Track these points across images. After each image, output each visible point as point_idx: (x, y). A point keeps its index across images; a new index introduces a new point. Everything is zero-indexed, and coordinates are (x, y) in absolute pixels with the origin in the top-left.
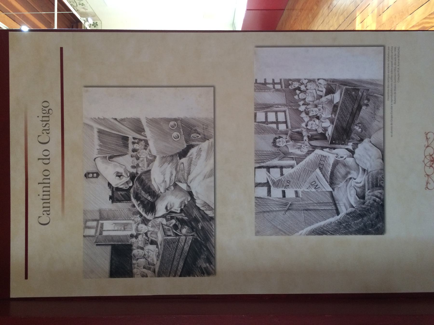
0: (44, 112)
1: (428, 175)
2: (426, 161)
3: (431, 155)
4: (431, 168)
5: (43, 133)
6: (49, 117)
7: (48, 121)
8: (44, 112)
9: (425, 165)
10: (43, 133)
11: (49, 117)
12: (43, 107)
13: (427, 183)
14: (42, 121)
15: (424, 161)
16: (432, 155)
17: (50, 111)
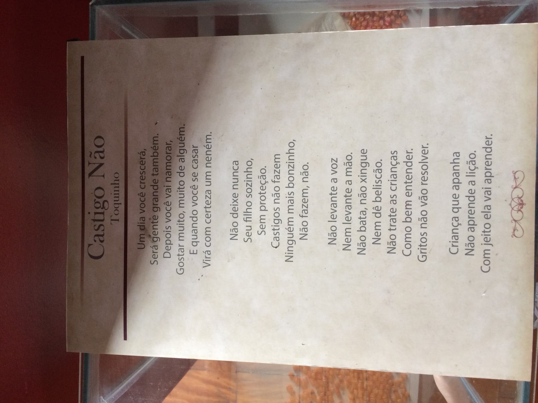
0: (98, 205)
1: (515, 221)
2: (514, 204)
3: (520, 198)
4: (519, 212)
5: (95, 241)
6: (103, 213)
7: (103, 220)
8: (98, 205)
9: (513, 209)
10: (95, 241)
11: (103, 213)
12: (96, 198)
13: (514, 230)
14: (94, 220)
15: (510, 205)
16: (522, 197)
17: (106, 203)
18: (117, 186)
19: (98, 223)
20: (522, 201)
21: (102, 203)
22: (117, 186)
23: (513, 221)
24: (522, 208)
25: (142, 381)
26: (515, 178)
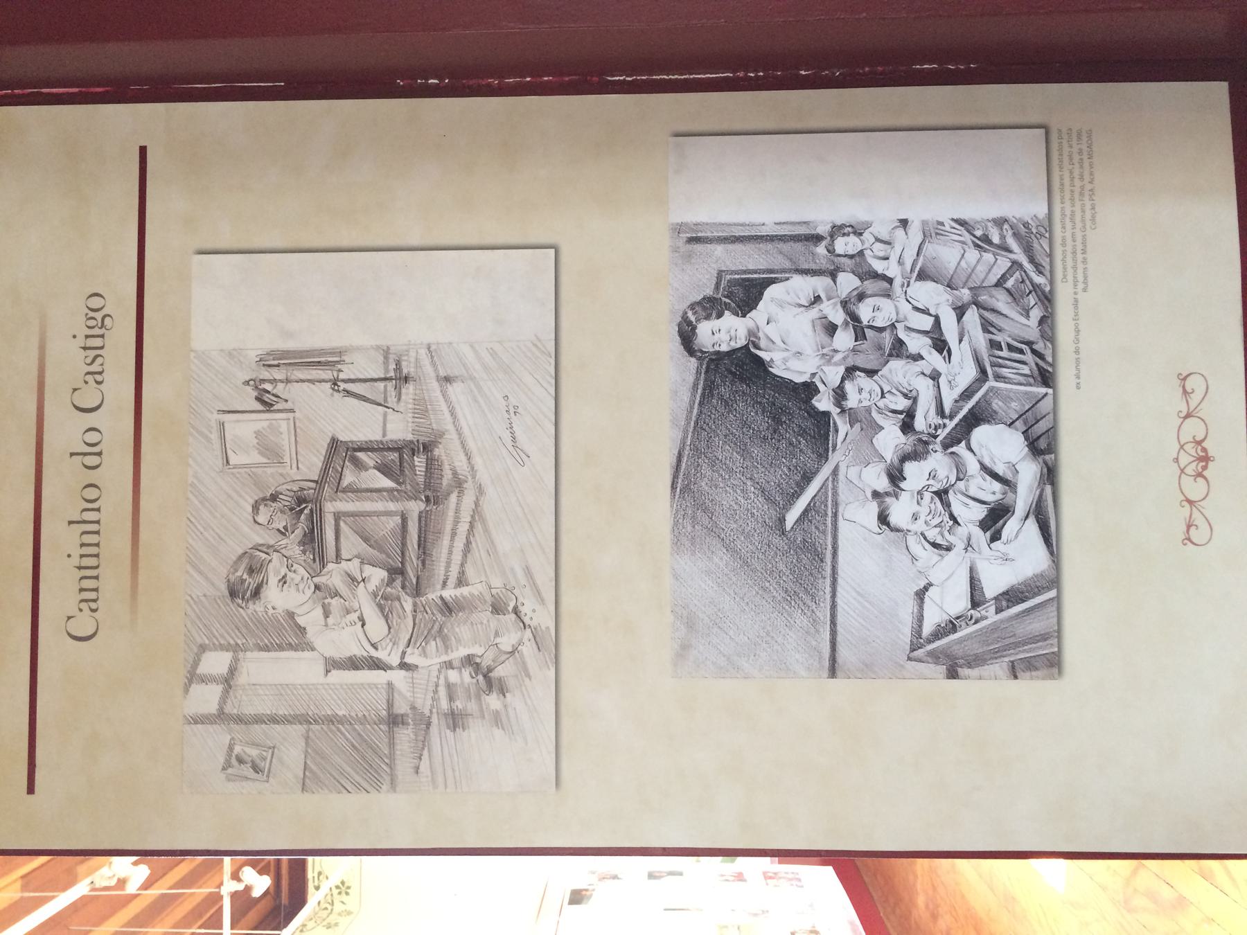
1: (1191, 502)
3: (1199, 443)
4: (1200, 480)
6: (102, 336)
9: (1182, 471)
11: (102, 336)
15: (1176, 460)
18: (94, 527)
19: (93, 353)
20: (1204, 450)
21: (100, 320)
22: (94, 527)
23: (1185, 503)
24: (1205, 468)
25: (201, 916)
26: (1185, 392)
